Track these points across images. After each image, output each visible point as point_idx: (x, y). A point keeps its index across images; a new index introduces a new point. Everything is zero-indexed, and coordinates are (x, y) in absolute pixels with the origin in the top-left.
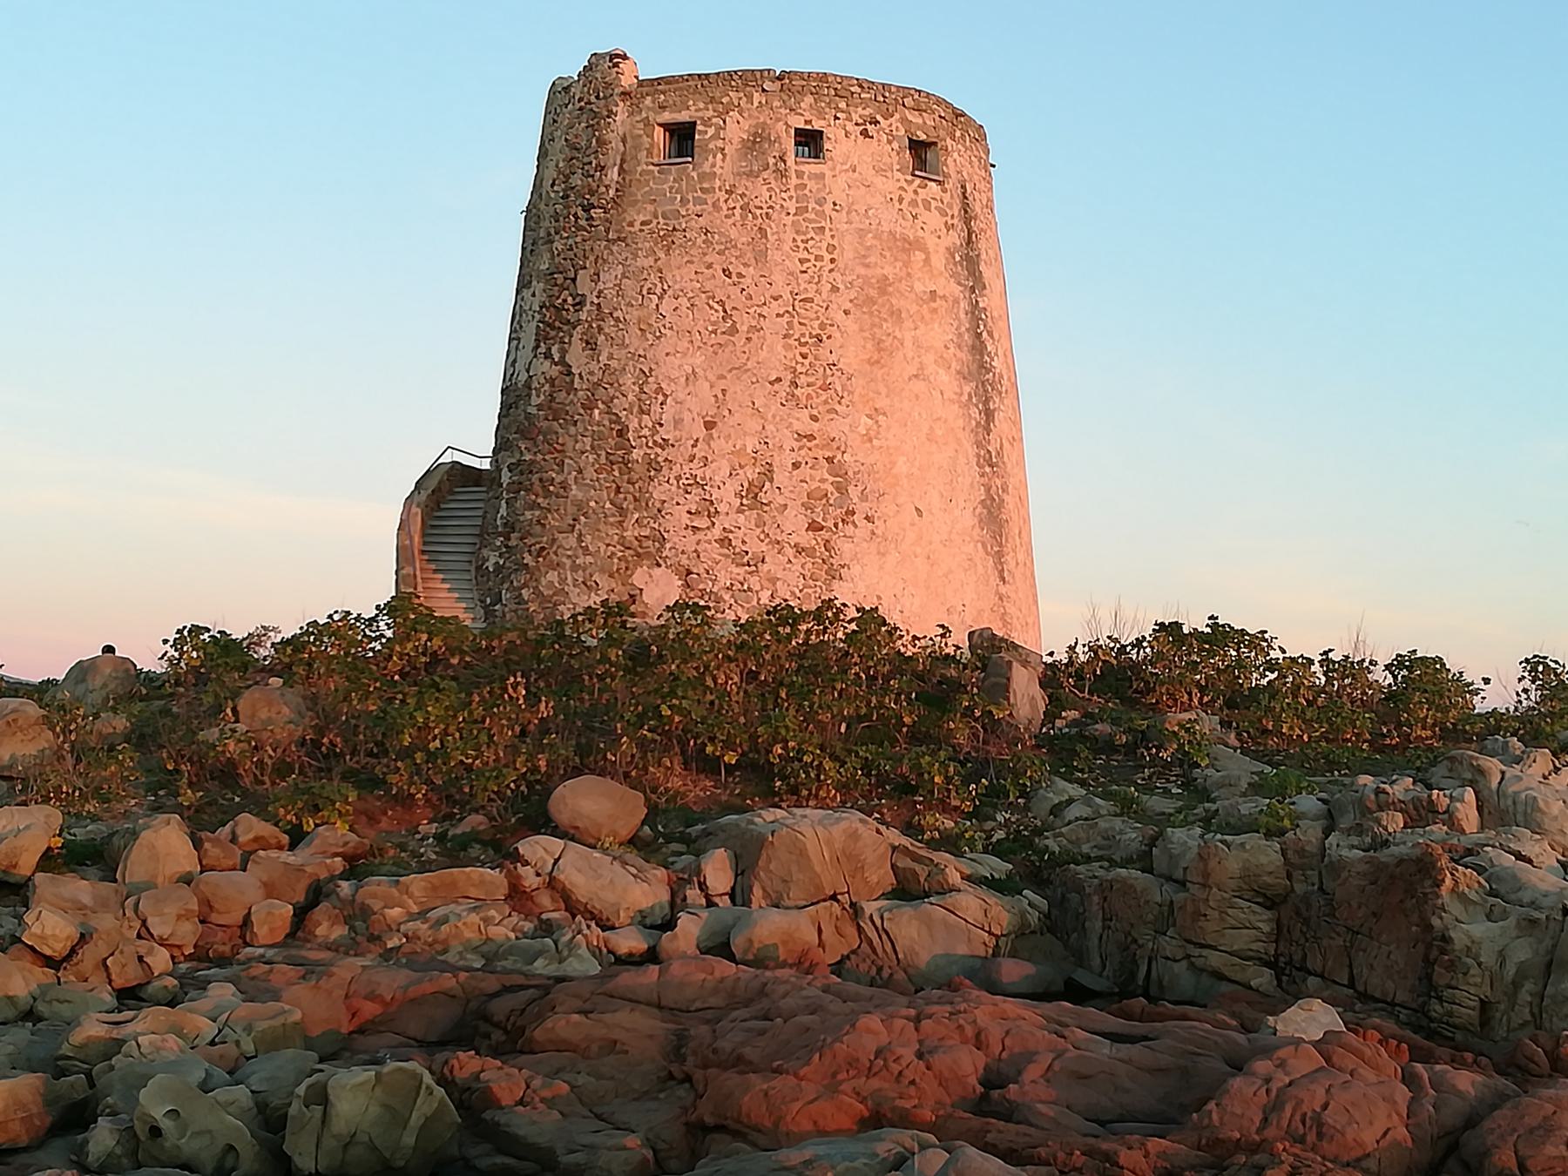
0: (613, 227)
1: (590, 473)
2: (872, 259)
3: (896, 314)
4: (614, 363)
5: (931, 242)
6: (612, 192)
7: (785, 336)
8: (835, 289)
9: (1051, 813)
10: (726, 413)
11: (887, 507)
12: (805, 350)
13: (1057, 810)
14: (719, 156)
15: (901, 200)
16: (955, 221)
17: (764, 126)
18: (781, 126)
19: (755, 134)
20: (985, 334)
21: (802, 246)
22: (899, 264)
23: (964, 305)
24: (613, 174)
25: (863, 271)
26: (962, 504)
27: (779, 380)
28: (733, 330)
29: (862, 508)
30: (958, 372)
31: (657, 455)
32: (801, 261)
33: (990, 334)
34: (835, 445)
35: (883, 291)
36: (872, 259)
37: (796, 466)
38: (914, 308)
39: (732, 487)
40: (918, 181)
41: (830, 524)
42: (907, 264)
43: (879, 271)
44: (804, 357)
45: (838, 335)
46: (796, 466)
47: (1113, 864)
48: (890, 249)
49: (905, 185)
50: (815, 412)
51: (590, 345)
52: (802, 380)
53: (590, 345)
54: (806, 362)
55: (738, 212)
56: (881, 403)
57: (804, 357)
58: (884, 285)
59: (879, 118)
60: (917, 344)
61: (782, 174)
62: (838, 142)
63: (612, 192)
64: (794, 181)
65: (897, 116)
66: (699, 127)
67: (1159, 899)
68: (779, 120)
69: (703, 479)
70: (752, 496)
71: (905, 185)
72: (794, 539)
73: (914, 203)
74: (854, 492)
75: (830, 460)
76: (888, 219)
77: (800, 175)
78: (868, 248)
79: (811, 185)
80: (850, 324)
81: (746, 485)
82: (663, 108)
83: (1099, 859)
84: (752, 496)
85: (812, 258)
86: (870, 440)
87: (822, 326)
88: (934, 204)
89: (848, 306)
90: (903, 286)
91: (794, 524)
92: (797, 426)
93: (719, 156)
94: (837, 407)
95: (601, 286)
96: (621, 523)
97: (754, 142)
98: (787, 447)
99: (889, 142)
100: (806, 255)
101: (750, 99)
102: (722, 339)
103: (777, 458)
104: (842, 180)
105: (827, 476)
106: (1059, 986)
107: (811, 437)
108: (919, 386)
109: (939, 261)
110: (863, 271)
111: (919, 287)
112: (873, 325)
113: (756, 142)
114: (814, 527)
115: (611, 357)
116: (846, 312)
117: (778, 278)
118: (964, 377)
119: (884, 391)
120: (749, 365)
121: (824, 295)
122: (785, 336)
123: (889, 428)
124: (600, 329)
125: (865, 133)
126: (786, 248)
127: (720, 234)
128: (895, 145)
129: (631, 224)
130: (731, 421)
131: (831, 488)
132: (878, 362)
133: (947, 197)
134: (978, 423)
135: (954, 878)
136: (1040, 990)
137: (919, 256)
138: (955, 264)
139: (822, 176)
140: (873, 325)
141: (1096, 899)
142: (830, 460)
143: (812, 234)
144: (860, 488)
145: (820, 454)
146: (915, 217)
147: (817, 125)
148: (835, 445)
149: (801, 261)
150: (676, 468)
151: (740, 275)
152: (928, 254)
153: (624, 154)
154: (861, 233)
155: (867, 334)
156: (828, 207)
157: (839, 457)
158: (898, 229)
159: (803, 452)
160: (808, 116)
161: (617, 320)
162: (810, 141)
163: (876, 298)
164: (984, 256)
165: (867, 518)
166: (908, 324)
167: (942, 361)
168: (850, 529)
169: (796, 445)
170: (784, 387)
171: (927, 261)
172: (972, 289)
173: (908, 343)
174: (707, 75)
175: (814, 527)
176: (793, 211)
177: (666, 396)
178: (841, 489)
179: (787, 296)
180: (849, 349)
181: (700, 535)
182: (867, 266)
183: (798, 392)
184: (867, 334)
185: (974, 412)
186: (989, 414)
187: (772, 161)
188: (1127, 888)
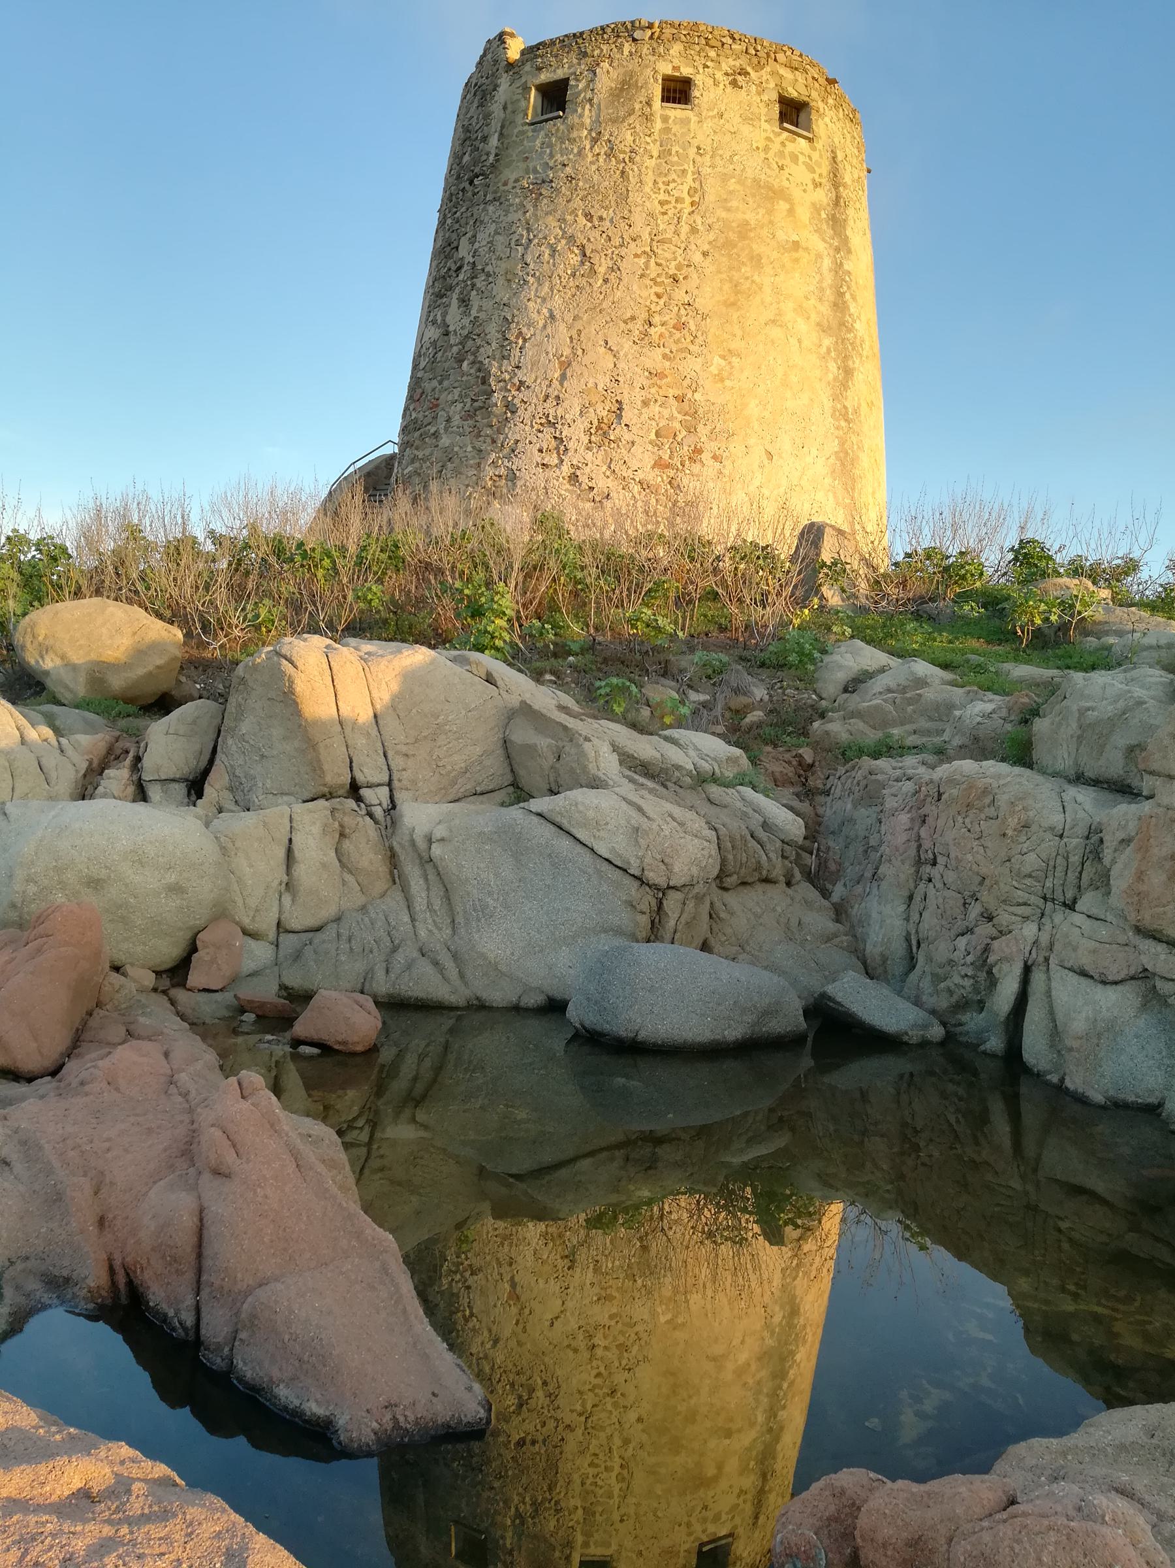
0: (491, 189)
1: (456, 421)
2: (734, 204)
3: (757, 261)
4: (482, 315)
5: (797, 193)
6: (491, 158)
7: (642, 276)
8: (694, 230)
9: (846, 690)
10: (580, 352)
11: (736, 447)
12: (659, 290)
13: (854, 685)
14: (588, 106)
15: (767, 149)
16: (824, 181)
17: (631, 74)
18: (649, 72)
19: (624, 82)
20: (848, 296)
21: (663, 187)
22: (762, 211)
23: (827, 263)
24: (494, 141)
25: (724, 215)
26: (814, 452)
27: (633, 318)
28: (593, 272)
29: (710, 447)
30: (818, 324)
31: (514, 397)
32: (661, 203)
33: (854, 298)
34: (685, 383)
35: (743, 236)
36: (734, 204)
37: (645, 403)
38: (775, 255)
39: (582, 424)
40: (786, 134)
41: (676, 461)
42: (770, 212)
43: (740, 216)
44: (659, 296)
45: (695, 276)
46: (645, 403)
47: (942, 754)
48: (754, 196)
49: (772, 136)
50: (667, 351)
51: (464, 302)
52: (656, 319)
53: (464, 302)
54: (662, 302)
55: (602, 159)
56: (735, 345)
57: (659, 296)
58: (744, 230)
59: (749, 69)
60: (777, 291)
61: (648, 118)
62: (706, 91)
63: (491, 158)
64: (658, 125)
65: (768, 69)
66: (572, 83)
67: (1056, 819)
68: (647, 66)
69: (556, 417)
70: (602, 433)
71: (772, 136)
72: (640, 476)
73: (781, 154)
74: (703, 431)
75: (680, 399)
76: (753, 166)
77: (665, 119)
78: (731, 192)
79: (675, 129)
80: (708, 266)
81: (595, 423)
82: (539, 69)
83: (916, 749)
84: (602, 433)
85: (673, 200)
86: (722, 380)
87: (679, 267)
88: (801, 159)
89: (706, 247)
90: (764, 232)
91: (642, 461)
92: (649, 364)
93: (588, 106)
94: (691, 347)
95: (477, 245)
96: (479, 464)
97: (622, 90)
98: (637, 385)
99: (759, 94)
100: (667, 198)
101: (620, 49)
102: (583, 282)
103: (626, 395)
104: (708, 125)
105: (676, 414)
106: (1072, 773)
107: (660, 375)
108: (776, 333)
109: (804, 214)
110: (724, 215)
111: (781, 235)
112: (731, 268)
113: (626, 87)
114: (659, 464)
115: (480, 309)
116: (705, 254)
117: (638, 218)
118: (824, 329)
119: (739, 333)
120: (604, 306)
121: (683, 236)
122: (642, 276)
123: (742, 370)
124: (473, 285)
125: (734, 83)
126: (647, 189)
127: (586, 181)
128: (765, 97)
129: (505, 184)
130: (586, 360)
131: (677, 425)
132: (733, 304)
133: (816, 156)
134: (835, 379)
135: (608, 764)
136: (734, 1032)
137: (783, 206)
138: (821, 220)
139: (688, 120)
140: (731, 268)
141: (904, 818)
142: (680, 399)
143: (674, 176)
144: (709, 427)
145: (671, 392)
146: (781, 168)
147: (686, 71)
148: (685, 383)
149: (661, 203)
150: (531, 409)
151: (601, 219)
152: (792, 204)
153: (504, 120)
154: (725, 178)
155: (724, 276)
156: (692, 151)
157: (689, 395)
158: (763, 177)
159: (653, 390)
160: (676, 62)
161: (488, 275)
162: (678, 91)
163: (735, 243)
164: (851, 222)
165: (715, 458)
166: (768, 270)
167: (800, 310)
168: (696, 468)
169: (646, 383)
170: (637, 327)
171: (791, 211)
172: (838, 250)
173: (767, 289)
174: (582, 34)
175: (659, 464)
176: (655, 154)
177: (525, 340)
178: (691, 430)
179: (646, 237)
180: (708, 294)
181: (549, 473)
182: (728, 210)
183: (652, 331)
184: (724, 276)
185: (833, 367)
186: (848, 372)
187: (637, 106)
188: (979, 800)
